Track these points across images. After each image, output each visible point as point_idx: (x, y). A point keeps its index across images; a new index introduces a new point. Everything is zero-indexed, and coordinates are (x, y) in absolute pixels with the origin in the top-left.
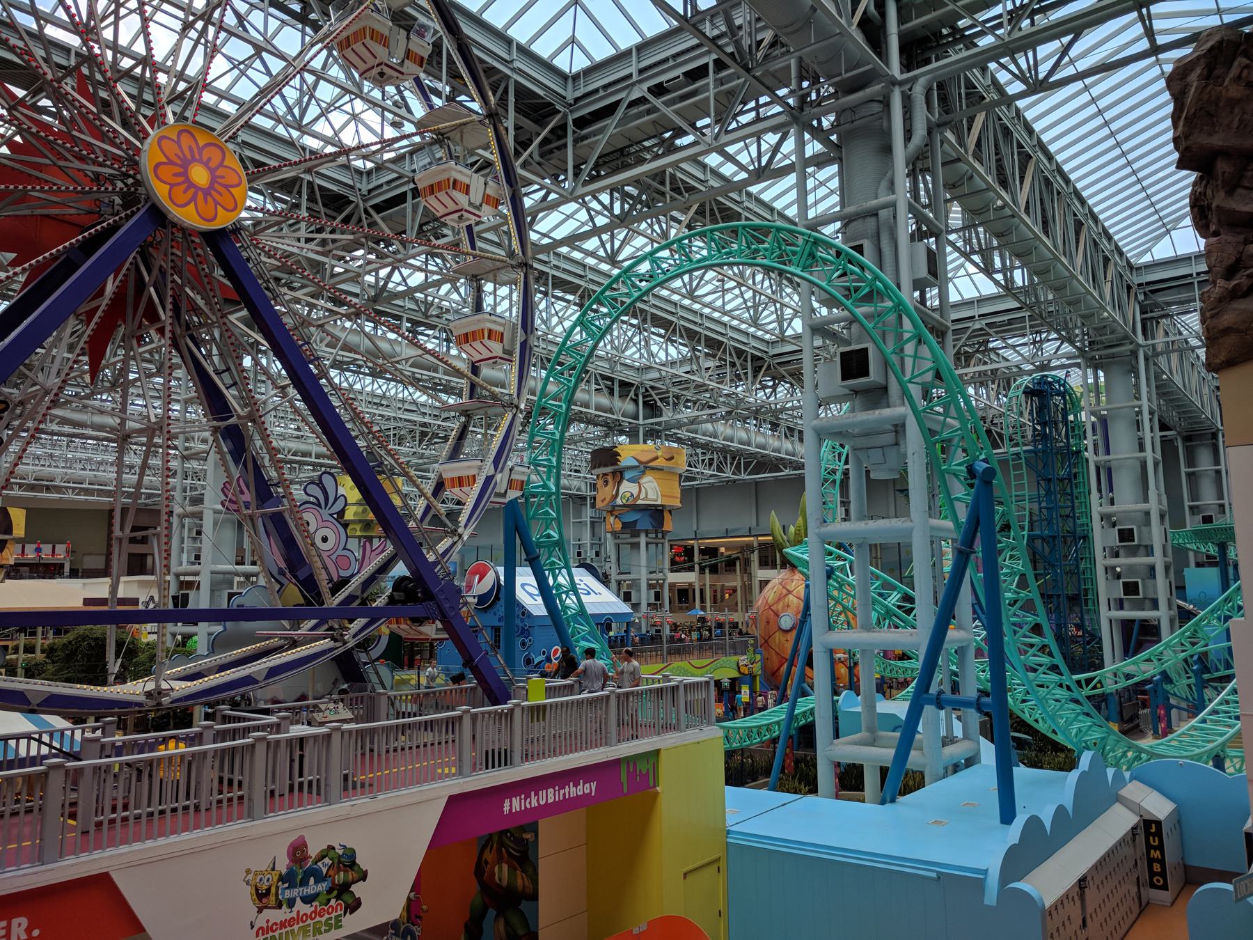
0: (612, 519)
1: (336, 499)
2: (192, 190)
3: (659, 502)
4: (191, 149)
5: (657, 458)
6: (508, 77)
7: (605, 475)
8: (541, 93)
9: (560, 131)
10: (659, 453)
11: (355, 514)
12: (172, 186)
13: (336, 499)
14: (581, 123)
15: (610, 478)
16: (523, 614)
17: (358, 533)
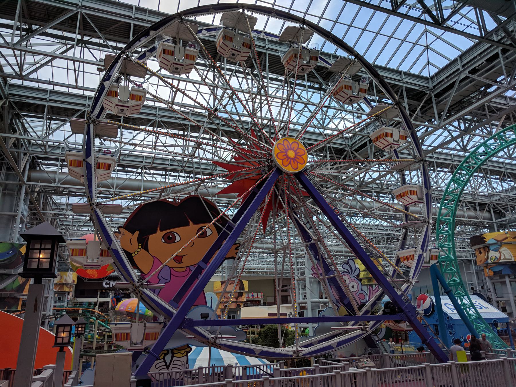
0: (487, 270)
1: (355, 270)
2: (289, 160)
3: (513, 260)
4: (287, 145)
5: (507, 238)
6: (402, 86)
7: (479, 249)
8: (417, 88)
9: (429, 101)
10: (508, 235)
11: (364, 275)
12: (283, 160)
13: (355, 270)
14: (438, 96)
15: (482, 250)
16: (448, 318)
17: (366, 283)
